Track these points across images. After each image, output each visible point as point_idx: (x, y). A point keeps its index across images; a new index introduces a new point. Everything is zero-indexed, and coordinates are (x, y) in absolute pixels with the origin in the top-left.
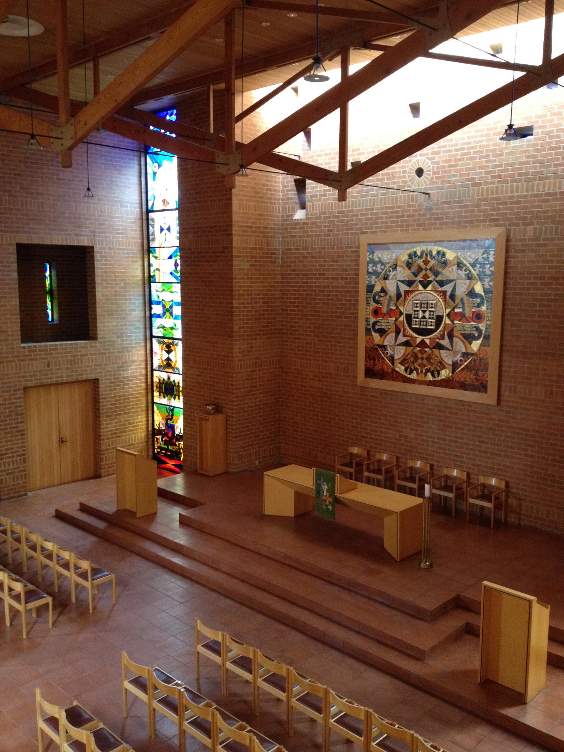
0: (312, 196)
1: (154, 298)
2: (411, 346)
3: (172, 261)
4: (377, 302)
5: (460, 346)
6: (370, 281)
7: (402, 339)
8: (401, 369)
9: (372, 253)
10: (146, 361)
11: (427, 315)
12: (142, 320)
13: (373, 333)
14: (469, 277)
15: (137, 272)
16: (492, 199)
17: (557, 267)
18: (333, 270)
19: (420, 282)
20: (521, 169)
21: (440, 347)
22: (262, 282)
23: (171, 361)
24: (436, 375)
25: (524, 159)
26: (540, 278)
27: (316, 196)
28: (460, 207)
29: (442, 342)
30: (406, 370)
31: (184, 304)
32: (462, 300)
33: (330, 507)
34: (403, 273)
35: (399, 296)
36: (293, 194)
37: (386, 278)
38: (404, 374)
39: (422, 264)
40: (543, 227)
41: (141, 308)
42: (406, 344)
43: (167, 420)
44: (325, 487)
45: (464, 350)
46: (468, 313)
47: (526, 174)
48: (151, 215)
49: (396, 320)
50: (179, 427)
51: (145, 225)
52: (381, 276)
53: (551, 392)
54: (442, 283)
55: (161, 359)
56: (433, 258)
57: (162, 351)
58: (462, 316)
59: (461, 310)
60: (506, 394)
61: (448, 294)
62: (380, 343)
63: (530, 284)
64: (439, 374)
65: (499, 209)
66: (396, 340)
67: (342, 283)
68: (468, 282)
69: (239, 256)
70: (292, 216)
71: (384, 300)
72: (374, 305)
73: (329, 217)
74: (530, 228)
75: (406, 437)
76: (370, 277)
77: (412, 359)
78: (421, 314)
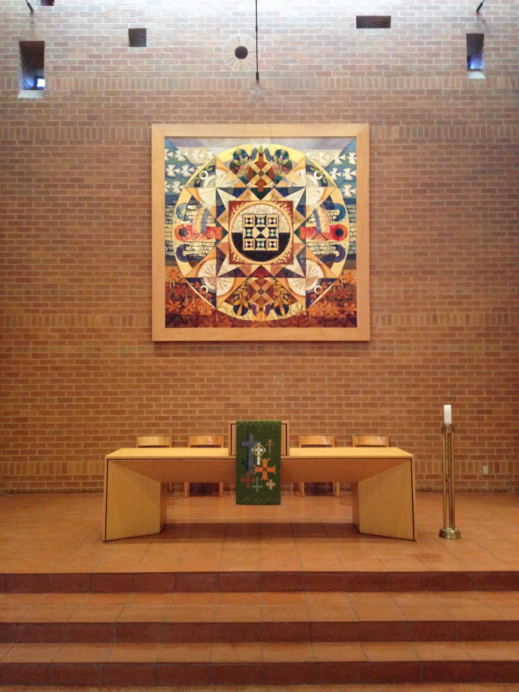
0: (55, 68)
5: (316, 270)
6: (171, 189)
7: (227, 267)
8: (227, 309)
11: (266, 233)
14: (323, 183)
16: (345, 93)
19: (253, 190)
21: (287, 274)
24: (283, 311)
27: (64, 68)
29: (289, 267)
32: (315, 212)
33: (271, 484)
34: (225, 179)
35: (220, 209)
37: (198, 185)
38: (233, 315)
39: (254, 167)
42: (236, 273)
44: (259, 450)
47: (386, 67)
49: (218, 241)
54: (285, 192)
56: (270, 158)
59: (314, 225)
61: (295, 205)
64: (287, 309)
67: (118, 192)
68: (322, 189)
77: (245, 294)
78: (256, 233)
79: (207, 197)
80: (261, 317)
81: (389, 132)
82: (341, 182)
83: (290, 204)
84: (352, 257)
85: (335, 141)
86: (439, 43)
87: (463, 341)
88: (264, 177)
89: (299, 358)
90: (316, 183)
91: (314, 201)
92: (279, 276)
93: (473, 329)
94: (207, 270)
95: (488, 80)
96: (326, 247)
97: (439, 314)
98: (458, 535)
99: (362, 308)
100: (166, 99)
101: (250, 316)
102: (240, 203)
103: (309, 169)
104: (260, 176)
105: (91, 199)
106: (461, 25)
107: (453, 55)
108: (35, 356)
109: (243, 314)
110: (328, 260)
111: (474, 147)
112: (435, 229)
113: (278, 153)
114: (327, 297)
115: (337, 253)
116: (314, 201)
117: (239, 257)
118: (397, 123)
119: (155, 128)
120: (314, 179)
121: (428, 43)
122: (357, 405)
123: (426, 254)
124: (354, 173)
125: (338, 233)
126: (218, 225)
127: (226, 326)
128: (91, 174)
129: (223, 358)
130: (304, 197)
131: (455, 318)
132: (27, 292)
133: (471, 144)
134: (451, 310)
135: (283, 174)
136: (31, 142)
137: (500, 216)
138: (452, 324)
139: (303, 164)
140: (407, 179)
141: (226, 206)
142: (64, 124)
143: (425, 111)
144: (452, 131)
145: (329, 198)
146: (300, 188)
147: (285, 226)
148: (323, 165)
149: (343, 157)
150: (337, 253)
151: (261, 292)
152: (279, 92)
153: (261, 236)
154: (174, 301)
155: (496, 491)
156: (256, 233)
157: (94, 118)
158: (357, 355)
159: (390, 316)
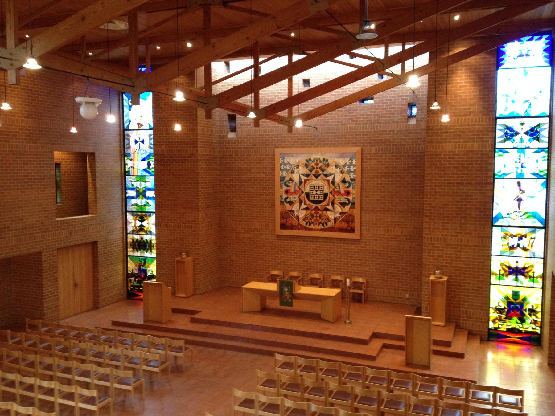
0: (240, 125)
1: (129, 185)
2: (309, 210)
3: (146, 162)
4: (288, 186)
5: (338, 209)
6: (282, 175)
7: (303, 206)
8: (303, 223)
9: (284, 159)
10: (123, 228)
11: (319, 192)
12: (120, 200)
13: (285, 204)
14: (342, 172)
15: (117, 168)
16: (353, 132)
17: (388, 167)
18: (257, 168)
19: (314, 175)
20: (368, 118)
21: (327, 210)
22: (211, 175)
23: (144, 226)
24: (325, 225)
25: (369, 113)
26: (380, 173)
27: (244, 125)
28: (335, 136)
29: (328, 207)
30: (307, 223)
31: (157, 188)
32: (338, 184)
33: (290, 300)
34: (303, 170)
35: (301, 182)
36: (227, 123)
37: (292, 173)
38: (306, 226)
39: (314, 165)
40: (381, 147)
41: (120, 192)
42: (307, 209)
43: (140, 267)
44: (286, 289)
45: (340, 211)
46: (342, 191)
47: (370, 121)
48: (126, 132)
49: (300, 196)
50: (152, 269)
51: (122, 138)
52: (290, 172)
53: (388, 230)
54: (326, 176)
55: (135, 226)
56: (321, 162)
57: (135, 221)
58: (339, 193)
59: (338, 190)
60: (364, 232)
61: (330, 181)
62: (290, 209)
63: (375, 176)
64: (326, 224)
65: (356, 138)
66: (300, 207)
67: (263, 175)
68: (341, 175)
69: (201, 160)
70: (227, 136)
71: (292, 185)
72: (285, 188)
73: (253, 138)
74: (373, 148)
75: (307, 261)
76: (282, 172)
77: (310, 217)
78: (315, 192)
79: (296, 177)
80: (316, 227)
81: (371, 149)
82: (349, 172)
83: (328, 181)
84: (353, 204)
85: (346, 154)
86: (395, 108)
87: (400, 241)
88: (318, 170)
89: (332, 244)
90: (339, 172)
91: (338, 179)
92: (323, 210)
93: (405, 236)
94: (295, 207)
95: (416, 124)
96: (343, 199)
97: (390, 229)
98: (351, 322)
99: (357, 225)
100: (281, 137)
101: (312, 226)
102: (308, 180)
103: (336, 166)
104: (317, 170)
105: (254, 178)
106: (405, 99)
107: (401, 113)
108: (236, 237)
109: (309, 225)
110: (343, 204)
111: (408, 156)
112: (390, 192)
113: (324, 159)
114: (343, 220)
115: (347, 202)
116: (338, 179)
117: (308, 202)
118: (374, 146)
119: (277, 150)
120: (338, 170)
121: (390, 108)
122: (355, 265)
123: (385, 203)
124: (355, 168)
125: (348, 193)
126: (300, 189)
127: (303, 230)
128: (254, 168)
129: (302, 242)
130: (334, 178)
131: (397, 231)
132: (233, 213)
133: (407, 155)
134: (396, 228)
135: (326, 168)
136: (232, 155)
137: (419, 187)
138: (395, 234)
139: (334, 164)
140: (378, 170)
141: (303, 181)
142: (244, 148)
143: (387, 140)
144: (399, 149)
145: (344, 178)
146: (332, 174)
147: (326, 190)
148: (341, 164)
149: (350, 161)
150: (347, 202)
151: (316, 217)
152: (325, 133)
153: (317, 194)
154: (284, 219)
155: (411, 305)
156: (315, 192)
157: (255, 145)
158: (355, 244)
159: (369, 229)
